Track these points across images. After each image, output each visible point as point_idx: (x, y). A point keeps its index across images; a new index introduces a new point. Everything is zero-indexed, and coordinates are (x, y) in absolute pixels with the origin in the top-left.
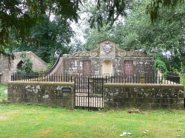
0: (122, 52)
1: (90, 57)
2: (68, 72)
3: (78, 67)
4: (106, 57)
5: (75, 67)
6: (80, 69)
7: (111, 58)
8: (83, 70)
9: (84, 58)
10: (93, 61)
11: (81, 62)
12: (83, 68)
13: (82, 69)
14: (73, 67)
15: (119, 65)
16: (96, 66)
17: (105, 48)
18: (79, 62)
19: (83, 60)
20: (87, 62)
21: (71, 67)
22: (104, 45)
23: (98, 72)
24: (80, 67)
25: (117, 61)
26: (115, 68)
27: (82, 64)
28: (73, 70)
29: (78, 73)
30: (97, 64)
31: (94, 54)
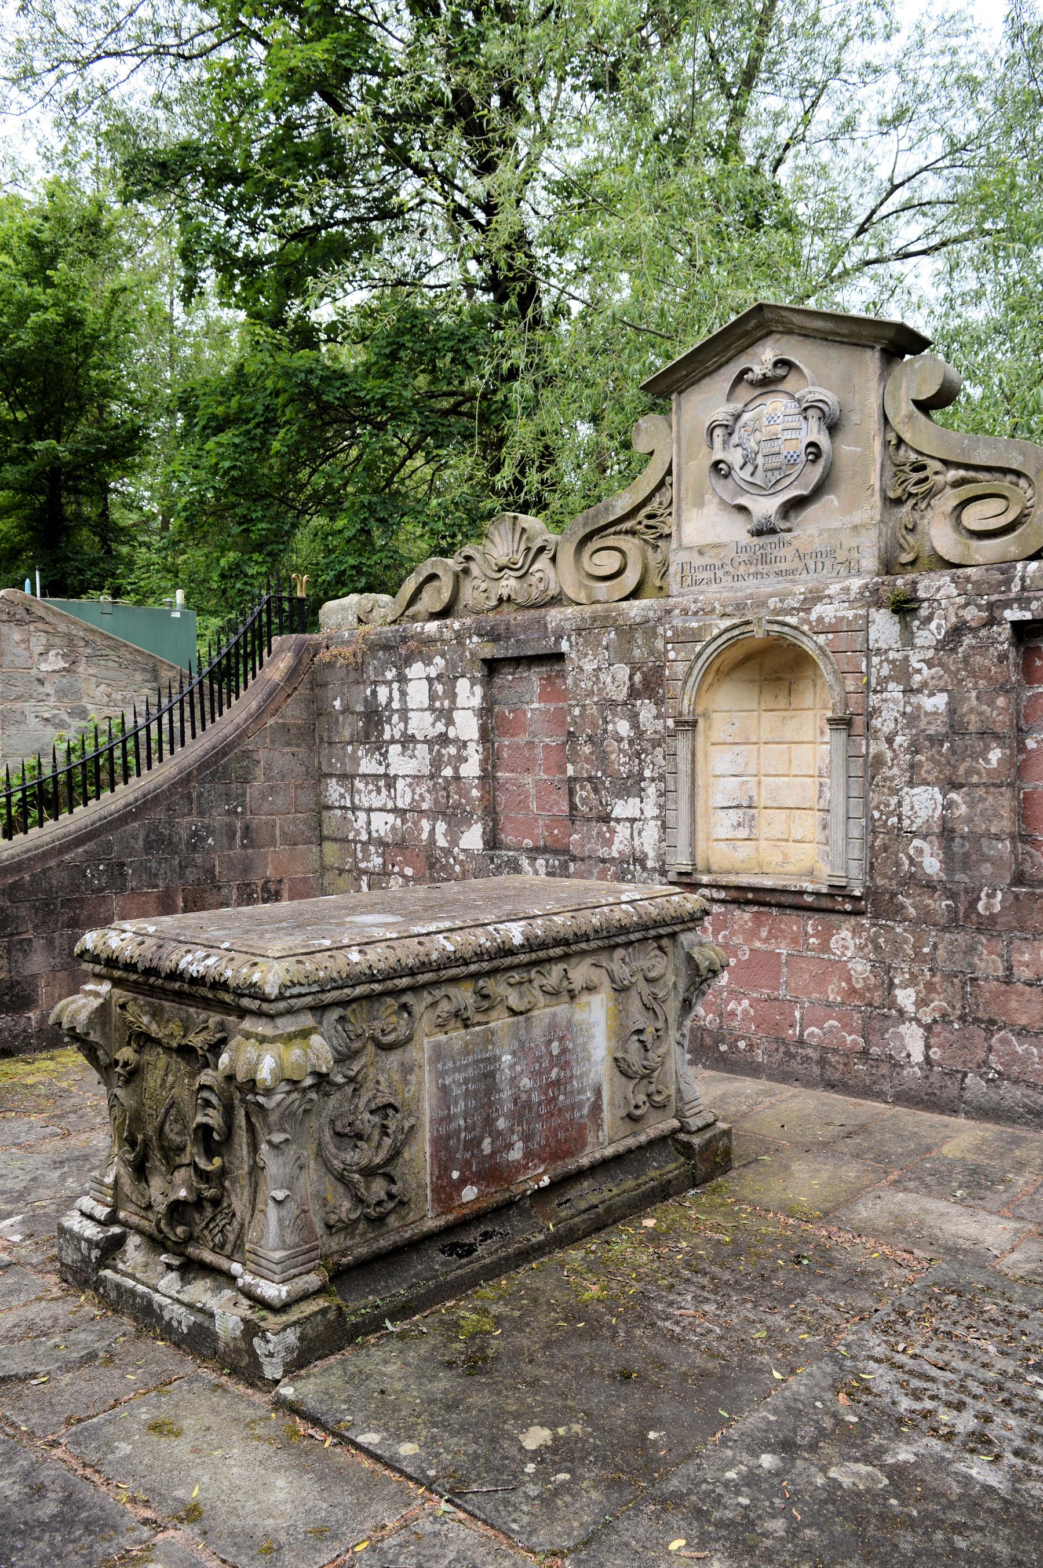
0: (987, 483)
1: (554, 616)
2: (354, 809)
3: (443, 739)
4: (751, 586)
5: (407, 741)
6: (456, 770)
7: (815, 597)
8: (487, 777)
9: (493, 636)
10: (589, 667)
11: (463, 686)
12: (491, 762)
13: (471, 769)
14: (393, 741)
15: (940, 701)
16: (623, 727)
17: (735, 457)
18: (448, 679)
19: (489, 651)
20: (535, 677)
21: (380, 747)
22: (721, 412)
23: (651, 811)
24: (456, 741)
25: (908, 639)
26: (878, 761)
27: (476, 701)
28: (391, 781)
29: (441, 827)
30: (634, 693)
31: (609, 562)
